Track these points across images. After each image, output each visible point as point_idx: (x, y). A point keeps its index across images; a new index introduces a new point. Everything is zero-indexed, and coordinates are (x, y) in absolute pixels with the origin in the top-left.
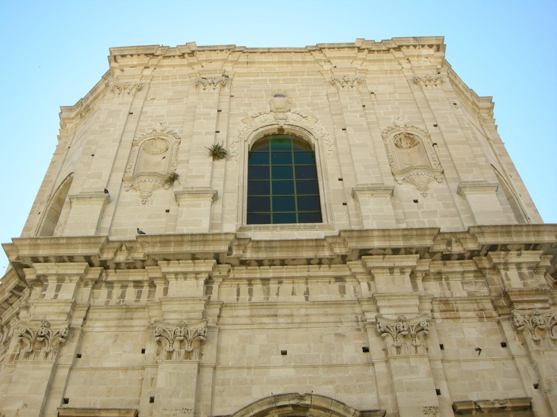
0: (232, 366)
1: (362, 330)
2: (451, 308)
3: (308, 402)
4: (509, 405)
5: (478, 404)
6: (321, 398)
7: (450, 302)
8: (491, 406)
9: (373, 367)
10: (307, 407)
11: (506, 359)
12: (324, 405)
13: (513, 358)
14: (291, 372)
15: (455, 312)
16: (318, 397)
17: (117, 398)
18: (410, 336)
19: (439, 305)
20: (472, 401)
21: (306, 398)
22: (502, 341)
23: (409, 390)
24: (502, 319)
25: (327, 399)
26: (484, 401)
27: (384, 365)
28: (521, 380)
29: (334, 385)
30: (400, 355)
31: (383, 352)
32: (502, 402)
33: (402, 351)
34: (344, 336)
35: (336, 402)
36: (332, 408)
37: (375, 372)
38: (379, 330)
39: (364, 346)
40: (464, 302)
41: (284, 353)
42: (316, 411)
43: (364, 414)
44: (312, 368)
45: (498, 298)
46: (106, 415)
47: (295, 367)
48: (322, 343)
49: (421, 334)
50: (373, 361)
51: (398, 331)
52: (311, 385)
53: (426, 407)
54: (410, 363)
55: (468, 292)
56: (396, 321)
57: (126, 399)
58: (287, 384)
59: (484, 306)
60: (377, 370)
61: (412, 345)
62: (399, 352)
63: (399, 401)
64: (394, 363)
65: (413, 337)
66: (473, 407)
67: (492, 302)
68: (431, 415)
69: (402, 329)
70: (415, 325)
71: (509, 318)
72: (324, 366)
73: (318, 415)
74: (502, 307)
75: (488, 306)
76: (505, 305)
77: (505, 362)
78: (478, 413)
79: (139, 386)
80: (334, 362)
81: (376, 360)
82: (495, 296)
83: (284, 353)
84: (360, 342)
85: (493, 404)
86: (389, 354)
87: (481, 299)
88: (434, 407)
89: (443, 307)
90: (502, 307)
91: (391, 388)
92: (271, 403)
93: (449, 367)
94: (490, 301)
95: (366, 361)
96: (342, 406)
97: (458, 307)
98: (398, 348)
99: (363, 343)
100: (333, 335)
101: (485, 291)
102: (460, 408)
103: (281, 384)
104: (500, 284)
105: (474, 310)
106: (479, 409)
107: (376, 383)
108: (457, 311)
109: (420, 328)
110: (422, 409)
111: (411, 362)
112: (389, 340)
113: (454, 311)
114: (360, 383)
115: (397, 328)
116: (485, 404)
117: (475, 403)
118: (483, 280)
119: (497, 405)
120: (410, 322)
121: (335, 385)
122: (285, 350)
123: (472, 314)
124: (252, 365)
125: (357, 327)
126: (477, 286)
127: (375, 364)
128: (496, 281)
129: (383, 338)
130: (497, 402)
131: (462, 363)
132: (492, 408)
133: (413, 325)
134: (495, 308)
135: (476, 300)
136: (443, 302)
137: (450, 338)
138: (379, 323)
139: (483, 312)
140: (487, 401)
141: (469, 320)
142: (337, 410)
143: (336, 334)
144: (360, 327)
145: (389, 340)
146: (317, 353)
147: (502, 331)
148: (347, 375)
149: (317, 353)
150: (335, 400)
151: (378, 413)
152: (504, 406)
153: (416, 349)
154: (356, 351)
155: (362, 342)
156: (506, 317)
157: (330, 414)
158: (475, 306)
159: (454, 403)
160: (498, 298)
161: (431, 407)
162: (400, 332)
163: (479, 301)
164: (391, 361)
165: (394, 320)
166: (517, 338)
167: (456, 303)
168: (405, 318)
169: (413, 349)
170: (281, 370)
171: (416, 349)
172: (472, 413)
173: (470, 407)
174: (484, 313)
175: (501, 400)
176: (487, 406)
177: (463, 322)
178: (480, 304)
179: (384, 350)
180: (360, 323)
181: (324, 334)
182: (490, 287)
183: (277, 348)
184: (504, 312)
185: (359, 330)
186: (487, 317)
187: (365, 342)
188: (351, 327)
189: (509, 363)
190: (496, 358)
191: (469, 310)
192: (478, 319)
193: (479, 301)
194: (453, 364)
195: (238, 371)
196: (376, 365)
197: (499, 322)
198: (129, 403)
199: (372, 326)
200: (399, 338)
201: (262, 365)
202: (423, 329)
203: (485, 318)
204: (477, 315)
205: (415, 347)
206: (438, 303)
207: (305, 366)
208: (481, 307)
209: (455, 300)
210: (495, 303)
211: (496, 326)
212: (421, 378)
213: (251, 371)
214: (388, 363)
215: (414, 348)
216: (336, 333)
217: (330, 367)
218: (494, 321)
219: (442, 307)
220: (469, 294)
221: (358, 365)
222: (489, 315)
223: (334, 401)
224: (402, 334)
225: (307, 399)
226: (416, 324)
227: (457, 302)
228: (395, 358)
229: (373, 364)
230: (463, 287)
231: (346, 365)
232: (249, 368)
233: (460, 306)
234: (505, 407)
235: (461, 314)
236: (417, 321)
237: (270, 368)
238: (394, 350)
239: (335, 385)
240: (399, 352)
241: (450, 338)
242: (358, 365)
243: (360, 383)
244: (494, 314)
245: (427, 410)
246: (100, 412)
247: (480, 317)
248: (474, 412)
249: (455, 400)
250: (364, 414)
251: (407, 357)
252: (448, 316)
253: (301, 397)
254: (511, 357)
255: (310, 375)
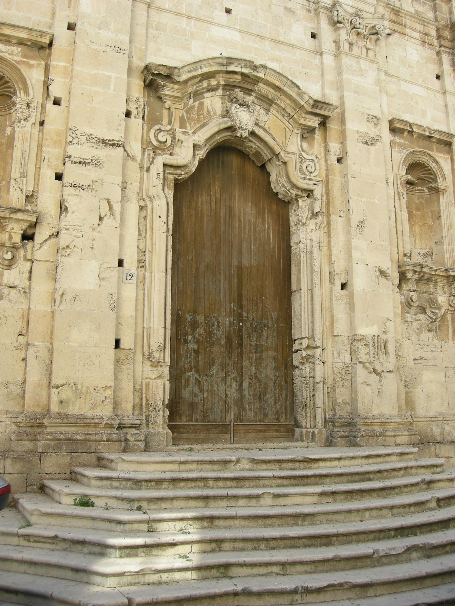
0: (169, 9)
1: (313, 12)
2: (400, 21)
3: (261, 75)
4: (437, 136)
5: (412, 127)
6: (276, 74)
7: (400, 14)
8: (422, 132)
9: (320, 57)
10: (257, 80)
11: (438, 92)
12: (278, 84)
13: (445, 93)
14: (235, 36)
15: (403, 27)
16: (273, 73)
17: (20, 14)
18: (363, 36)
19: (390, 13)
20: (408, 122)
21: (260, 70)
22: (437, 72)
23: (356, 92)
24: (444, 51)
25: (282, 78)
26: (419, 125)
27: (332, 58)
28: (448, 116)
29: (280, 65)
30: (352, 53)
31: (334, 44)
32: (432, 132)
33: (355, 48)
34: (294, 12)
35: (290, 83)
36: (285, 89)
37: (322, 64)
38: (336, 19)
39: (312, 31)
40: (413, 19)
41: (228, 11)
42: (265, 87)
43: (317, 104)
44: (258, 39)
45: (444, 28)
46: (11, 33)
47: (240, 31)
48: (270, 12)
49: (374, 37)
50: (323, 50)
51: (352, 26)
52: (257, 57)
53: (369, 115)
54: (360, 65)
55: (415, 10)
56: (352, 15)
57: (33, 18)
58: (231, 48)
59: (429, 31)
60: (325, 61)
61: (365, 46)
62: (351, 49)
63: (346, 100)
64: (346, 60)
65: (365, 38)
66: (408, 128)
67: (438, 30)
68: (373, 124)
69: (358, 26)
70: (370, 26)
71: (449, 52)
72: (272, 40)
73: (267, 92)
74: (445, 39)
75: (433, 33)
76: (449, 38)
77: (436, 94)
78: (409, 136)
79: (50, 5)
80: (282, 39)
81: (326, 51)
82: (442, 25)
83: (228, 11)
84: (310, 25)
85: (425, 131)
86: (341, 48)
87: (428, 23)
88: (376, 117)
89: (392, 16)
90: (445, 39)
91: (339, 85)
92: (222, 65)
93: (390, 82)
94: (435, 28)
95: (314, 48)
96: (296, 89)
97: (406, 22)
98: (351, 44)
99: (312, 28)
100: (283, 8)
101: (431, 16)
102: (397, 125)
103: (224, 47)
104: (446, 14)
105: (420, 32)
106: (411, 132)
107: (323, 75)
108: (405, 26)
109: (374, 31)
110: (366, 116)
111: (361, 64)
112: (343, 34)
113: (402, 25)
114: (306, 70)
115: (353, 23)
116: (418, 129)
117: (410, 125)
118: (431, 4)
119: (427, 134)
120: (364, 21)
121: (281, 65)
122: (231, 8)
123: (416, 35)
124: (193, 15)
125: (308, 7)
126: (425, 8)
127: (324, 54)
128: (444, 9)
129: (337, 29)
130: (428, 130)
131: (401, 81)
132: (423, 134)
133: (367, 25)
134: (439, 37)
135: (424, 21)
136: (394, 12)
137: (394, 52)
138: (337, 11)
139: (427, 37)
140: (421, 126)
141: (413, 40)
142: (290, 92)
143: (285, 8)
144: (311, 8)
145: (343, 34)
146: (264, 23)
147: (441, 64)
148: (294, 58)
149: (264, 23)
150: (291, 81)
151: (330, 107)
152: (432, 135)
153: (367, 52)
154: (305, 34)
155: (311, 26)
156: (448, 50)
157: (280, 94)
158: (420, 28)
159: (393, 119)
160: (444, 28)
161: (374, 116)
162: (354, 28)
163: (426, 24)
164: (343, 56)
165: (350, 12)
166: (452, 75)
167: (405, 18)
168: (363, 15)
169: (364, 50)
170: (225, 30)
171: (367, 52)
172: (403, 133)
173: (405, 128)
174: (428, 38)
175: (431, 130)
176: (419, 131)
177: (408, 40)
178: (426, 28)
179: (335, 42)
180: (311, 4)
181: (273, 3)
182: (437, 13)
183: (222, 3)
184: (446, 45)
185: (309, 11)
186: (428, 44)
187: (315, 27)
188: (301, 5)
189: (440, 96)
190: (430, 87)
191: (415, 30)
192: (420, 42)
193: (426, 24)
194: (394, 80)
195: (176, 17)
196: (324, 56)
197: (438, 53)
198: (38, 24)
199: (325, 11)
200: (352, 34)
201: (203, 18)
202: (377, 33)
203: (427, 44)
204: (421, 38)
205: (367, 49)
206: (389, 10)
207: (251, 33)
208: (427, 31)
209: (406, 14)
210: (441, 32)
211: (435, 56)
212: (368, 84)
213: (191, 21)
214: (336, 58)
215: (365, 50)
216: (286, 7)
217: (278, 43)
218: (434, 50)
219: (393, 17)
220: (417, 12)
221: (306, 50)
222: (431, 42)
223: (289, 82)
224: (357, 31)
225: (261, 72)
226: (371, 25)
227: (407, 17)
228: (346, 54)
229: (321, 54)
230: (412, 3)
231: (294, 46)
232: (189, 17)
233: (408, 22)
234: (433, 137)
235: (408, 31)
236: (374, 23)
237: (213, 24)
238: (347, 45)
239: (281, 65)
240: (351, 49)
241: (394, 52)
242: (306, 50)
243: (306, 70)
244: (436, 43)
245: (370, 118)
246: (3, 27)
247: (422, 41)
248: (406, 133)
249: (395, 117)
250: (317, 104)
251: (358, 57)
252: (395, 28)
253: (255, 68)
254: (443, 92)
255: (256, 46)
